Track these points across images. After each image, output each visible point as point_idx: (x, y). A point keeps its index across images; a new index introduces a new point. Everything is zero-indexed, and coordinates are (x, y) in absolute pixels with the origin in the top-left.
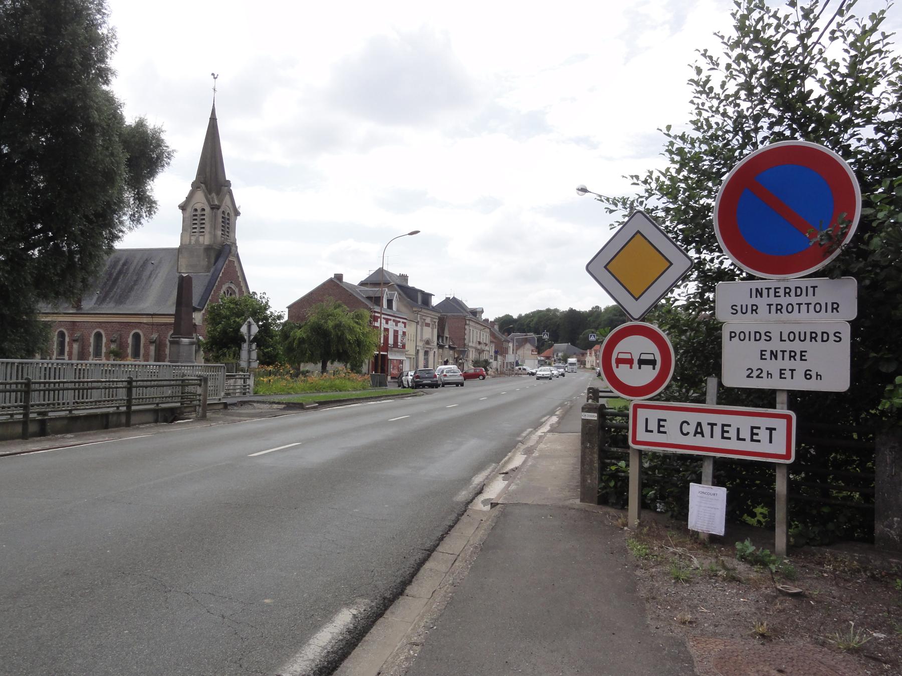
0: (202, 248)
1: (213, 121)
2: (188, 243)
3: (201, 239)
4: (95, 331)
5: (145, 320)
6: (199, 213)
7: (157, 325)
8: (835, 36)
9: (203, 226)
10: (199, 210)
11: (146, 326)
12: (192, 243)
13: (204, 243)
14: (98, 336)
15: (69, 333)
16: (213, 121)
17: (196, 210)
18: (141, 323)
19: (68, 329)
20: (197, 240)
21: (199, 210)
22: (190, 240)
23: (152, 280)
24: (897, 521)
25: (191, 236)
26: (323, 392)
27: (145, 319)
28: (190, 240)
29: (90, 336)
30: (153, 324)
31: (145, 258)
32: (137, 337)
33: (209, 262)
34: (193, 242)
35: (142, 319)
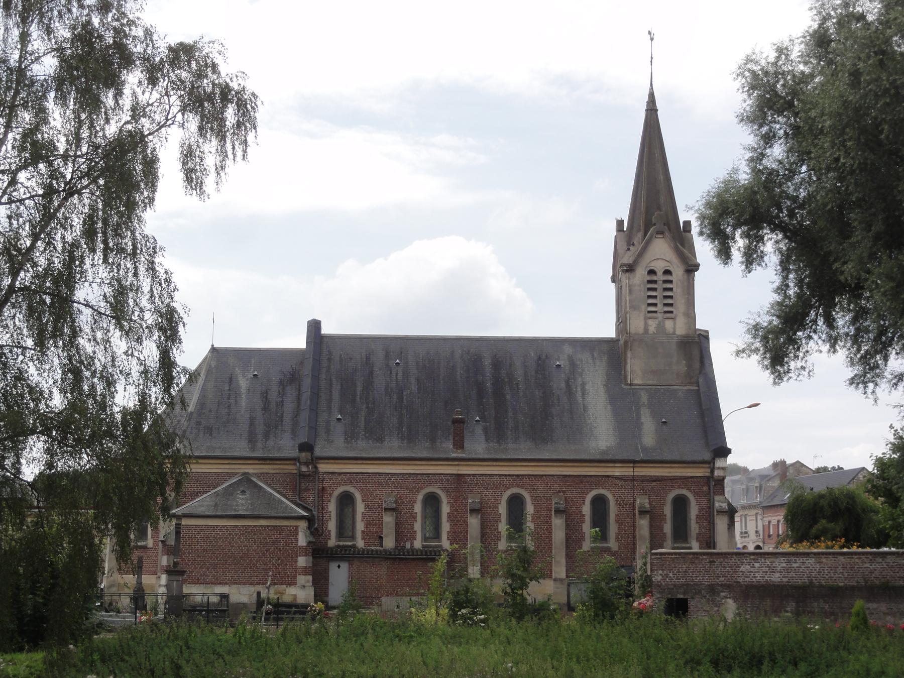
0: (675, 340)
1: (652, 96)
2: (641, 331)
3: (669, 324)
4: (509, 493)
5: (617, 471)
6: (660, 277)
7: (642, 481)
8: (130, 248)
9: (669, 301)
10: (660, 273)
11: (620, 483)
12: (650, 332)
13: (674, 333)
14: (516, 503)
15: (448, 496)
16: (652, 96)
17: (652, 272)
18: (607, 476)
19: (445, 489)
20: (661, 327)
21: (660, 273)
22: (646, 325)
23: (579, 394)
24: (32, 521)
25: (646, 319)
26: (323, 523)
27: (617, 470)
28: (646, 325)
29: (497, 502)
30: (633, 479)
31: (364, 356)
32: (600, 503)
33: (689, 366)
34: (652, 328)
35: (610, 469)
